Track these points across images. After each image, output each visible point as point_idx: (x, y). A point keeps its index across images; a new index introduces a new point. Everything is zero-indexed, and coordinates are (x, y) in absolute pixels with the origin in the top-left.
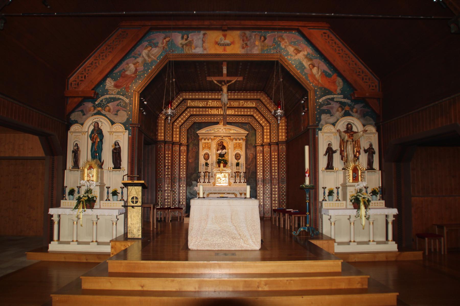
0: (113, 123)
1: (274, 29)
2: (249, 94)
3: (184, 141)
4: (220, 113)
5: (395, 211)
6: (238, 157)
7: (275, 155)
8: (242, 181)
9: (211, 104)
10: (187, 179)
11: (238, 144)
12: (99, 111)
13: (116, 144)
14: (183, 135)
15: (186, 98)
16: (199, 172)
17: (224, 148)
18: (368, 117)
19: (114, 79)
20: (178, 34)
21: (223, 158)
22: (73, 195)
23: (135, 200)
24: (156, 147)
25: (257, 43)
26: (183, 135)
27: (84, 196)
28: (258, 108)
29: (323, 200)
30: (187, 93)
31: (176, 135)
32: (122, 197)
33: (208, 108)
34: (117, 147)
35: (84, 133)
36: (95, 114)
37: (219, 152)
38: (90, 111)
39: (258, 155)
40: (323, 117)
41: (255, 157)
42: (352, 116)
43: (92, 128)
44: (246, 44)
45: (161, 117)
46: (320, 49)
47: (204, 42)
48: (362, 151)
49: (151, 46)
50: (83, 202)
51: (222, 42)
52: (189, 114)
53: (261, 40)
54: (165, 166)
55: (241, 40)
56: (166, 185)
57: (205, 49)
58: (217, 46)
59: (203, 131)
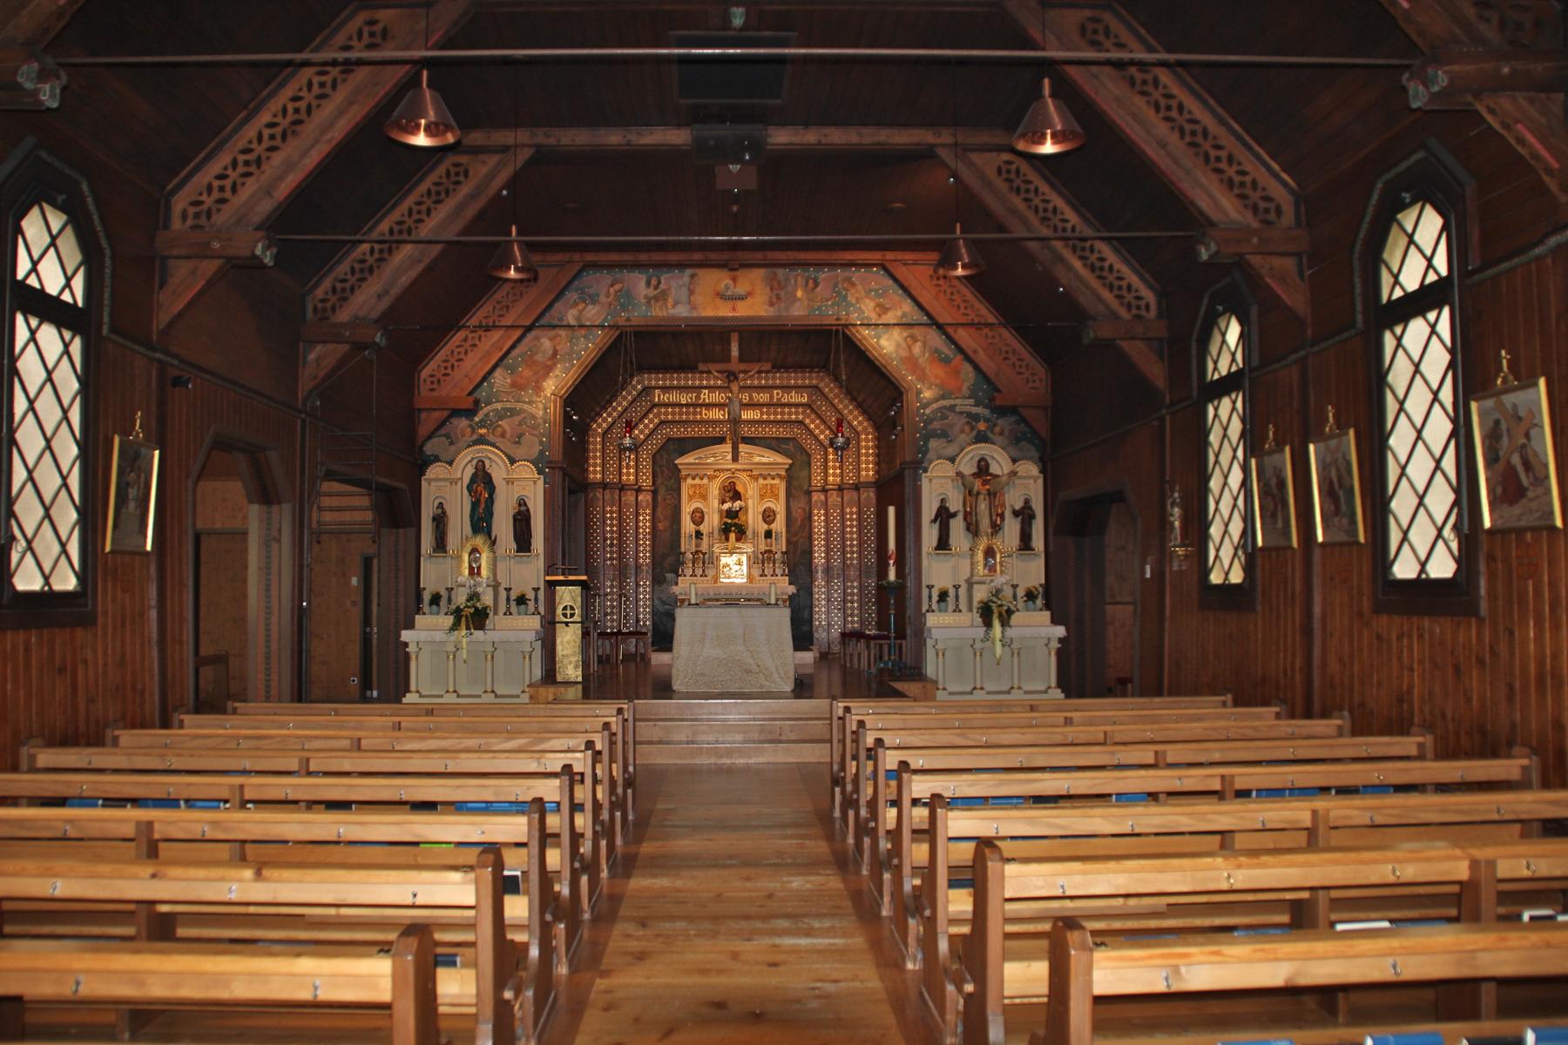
0: (513, 461)
1: (832, 265)
3: (647, 482)
5: (1060, 631)
7: (852, 511)
8: (779, 571)
10: (653, 569)
12: (481, 435)
13: (522, 503)
14: (644, 467)
16: (681, 553)
17: (737, 496)
18: (1024, 443)
19: (512, 370)
20: (640, 276)
21: (736, 521)
22: (438, 605)
23: (568, 612)
24: (586, 498)
25: (799, 294)
26: (644, 467)
27: (467, 606)
28: (814, 407)
29: (928, 611)
32: (536, 608)
33: (701, 405)
34: (523, 508)
35: (453, 482)
36: (476, 443)
37: (726, 506)
38: (463, 436)
39: (816, 512)
40: (933, 443)
41: (809, 518)
42: (993, 443)
43: (470, 471)
44: (778, 297)
45: (595, 430)
46: (925, 305)
47: (691, 292)
48: (1008, 514)
49: (584, 302)
50: (466, 616)
51: (729, 293)
53: (743, 504)
54: (605, 539)
56: (609, 583)
57: (694, 308)
58: (718, 301)
59: (689, 459)
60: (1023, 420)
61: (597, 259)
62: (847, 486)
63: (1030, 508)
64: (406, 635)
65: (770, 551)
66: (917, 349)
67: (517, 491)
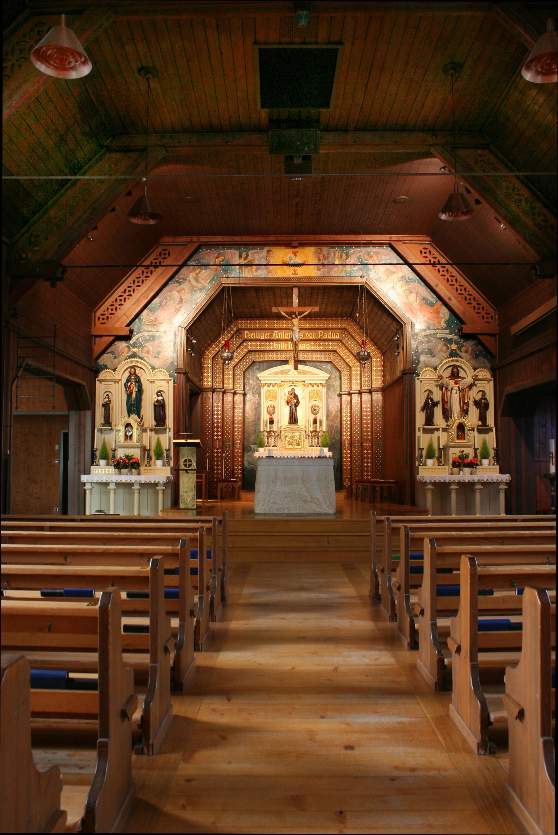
2: (330, 321)
4: (289, 348)
6: (315, 410)
9: (277, 335)
11: (315, 391)
12: (134, 353)
15: (241, 328)
20: (235, 251)
23: (188, 463)
28: (344, 341)
30: (243, 320)
31: (228, 379)
33: (273, 340)
34: (160, 398)
35: (116, 382)
36: (130, 357)
43: (127, 374)
48: (471, 403)
52: (246, 350)
55: (317, 259)
60: (480, 342)
61: (207, 240)
62: (364, 391)
63: (486, 399)
64: (84, 478)
65: (316, 431)
66: (412, 297)
67: (158, 386)
